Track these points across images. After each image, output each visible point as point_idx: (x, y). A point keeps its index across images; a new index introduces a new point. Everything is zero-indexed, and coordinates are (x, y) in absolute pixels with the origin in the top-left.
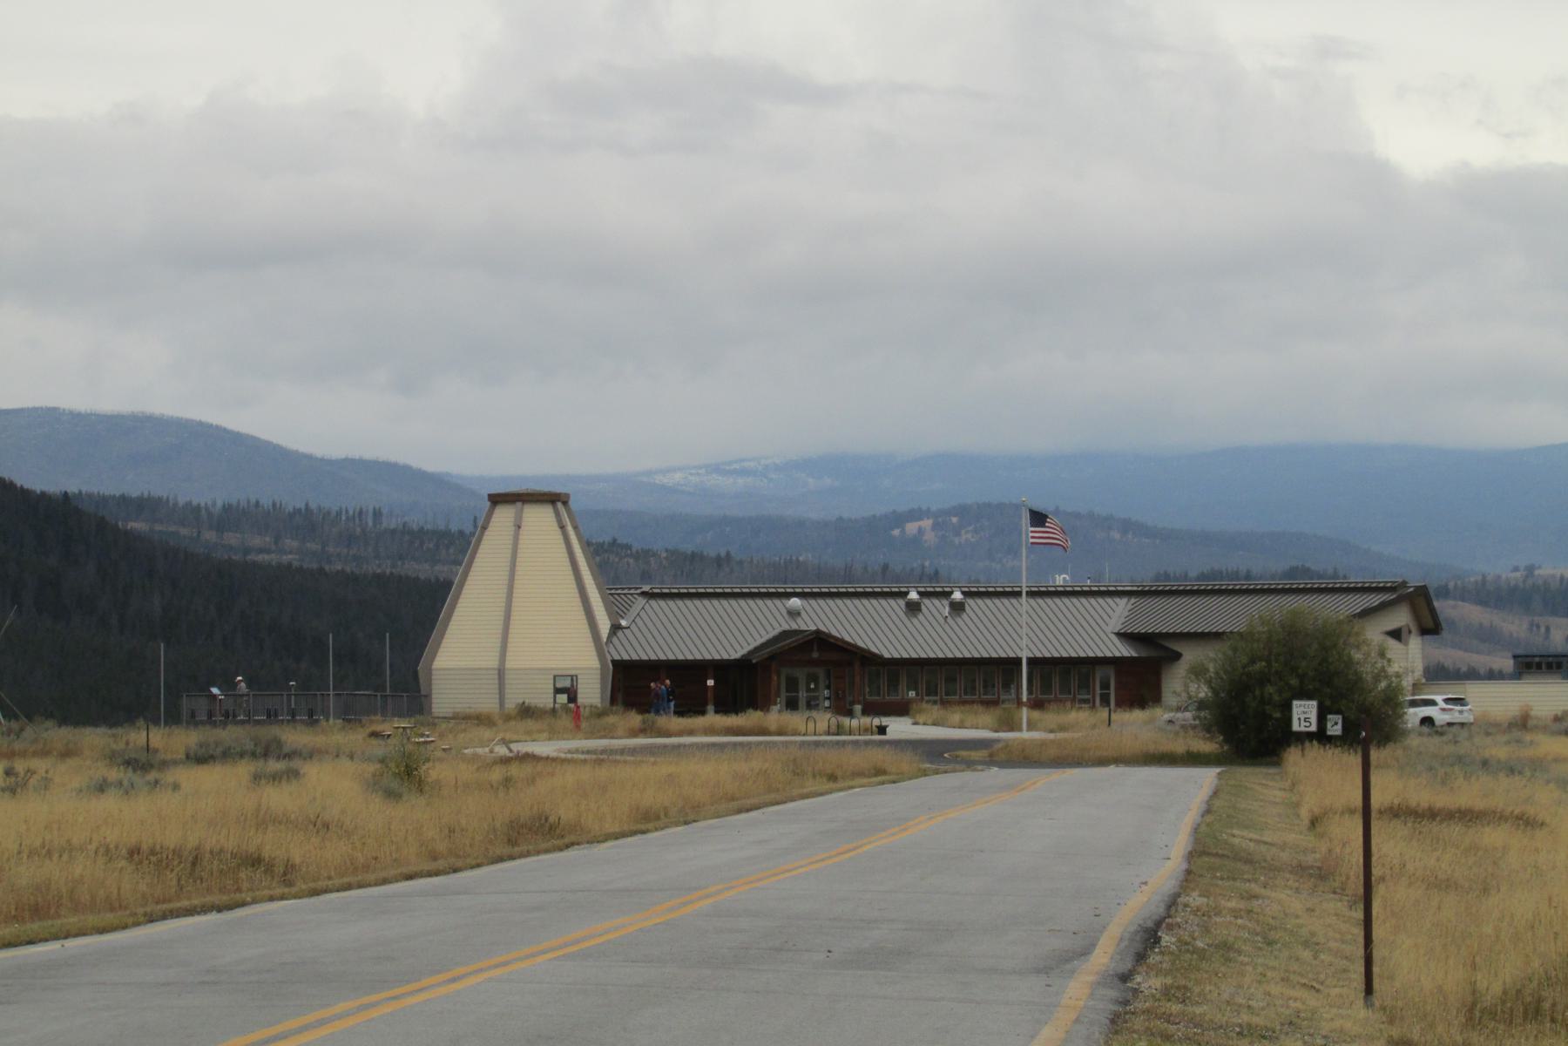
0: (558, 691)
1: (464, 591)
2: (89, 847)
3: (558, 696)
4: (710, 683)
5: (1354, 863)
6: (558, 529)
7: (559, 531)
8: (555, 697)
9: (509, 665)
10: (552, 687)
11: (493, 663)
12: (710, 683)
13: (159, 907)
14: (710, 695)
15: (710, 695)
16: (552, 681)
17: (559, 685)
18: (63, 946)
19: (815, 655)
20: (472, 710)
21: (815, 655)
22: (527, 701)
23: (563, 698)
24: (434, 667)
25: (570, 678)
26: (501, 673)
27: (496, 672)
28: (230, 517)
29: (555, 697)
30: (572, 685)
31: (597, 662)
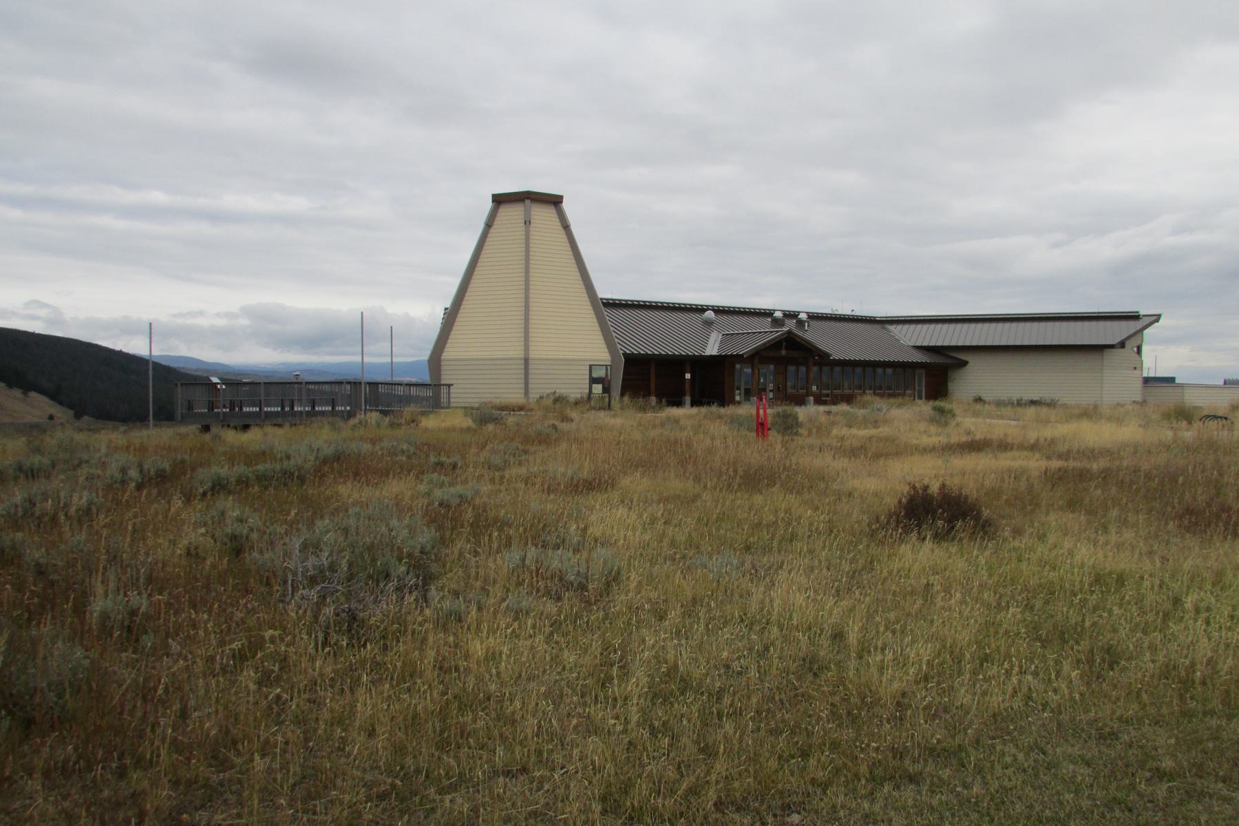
0: (594, 381)
1: (458, 319)
2: (907, 762)
3: (594, 386)
4: (688, 376)
5: (823, 559)
6: (561, 228)
7: (563, 232)
8: (590, 388)
9: (532, 355)
10: (588, 377)
11: (518, 353)
12: (688, 376)
13: (854, 431)
14: (687, 387)
15: (687, 387)
16: (588, 372)
17: (594, 375)
18: (771, 391)
19: (783, 352)
20: (498, 401)
21: (783, 352)
22: (558, 391)
23: (598, 389)
24: (443, 357)
25: (604, 367)
26: (526, 361)
27: (523, 362)
28: (196, 370)
29: (590, 388)
30: (607, 375)
31: (608, 354)
